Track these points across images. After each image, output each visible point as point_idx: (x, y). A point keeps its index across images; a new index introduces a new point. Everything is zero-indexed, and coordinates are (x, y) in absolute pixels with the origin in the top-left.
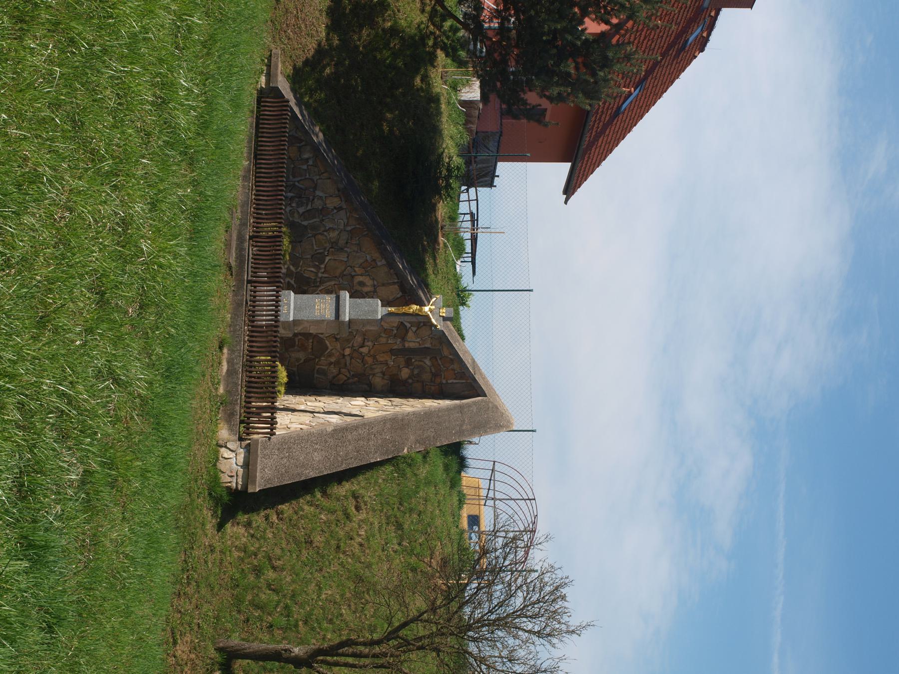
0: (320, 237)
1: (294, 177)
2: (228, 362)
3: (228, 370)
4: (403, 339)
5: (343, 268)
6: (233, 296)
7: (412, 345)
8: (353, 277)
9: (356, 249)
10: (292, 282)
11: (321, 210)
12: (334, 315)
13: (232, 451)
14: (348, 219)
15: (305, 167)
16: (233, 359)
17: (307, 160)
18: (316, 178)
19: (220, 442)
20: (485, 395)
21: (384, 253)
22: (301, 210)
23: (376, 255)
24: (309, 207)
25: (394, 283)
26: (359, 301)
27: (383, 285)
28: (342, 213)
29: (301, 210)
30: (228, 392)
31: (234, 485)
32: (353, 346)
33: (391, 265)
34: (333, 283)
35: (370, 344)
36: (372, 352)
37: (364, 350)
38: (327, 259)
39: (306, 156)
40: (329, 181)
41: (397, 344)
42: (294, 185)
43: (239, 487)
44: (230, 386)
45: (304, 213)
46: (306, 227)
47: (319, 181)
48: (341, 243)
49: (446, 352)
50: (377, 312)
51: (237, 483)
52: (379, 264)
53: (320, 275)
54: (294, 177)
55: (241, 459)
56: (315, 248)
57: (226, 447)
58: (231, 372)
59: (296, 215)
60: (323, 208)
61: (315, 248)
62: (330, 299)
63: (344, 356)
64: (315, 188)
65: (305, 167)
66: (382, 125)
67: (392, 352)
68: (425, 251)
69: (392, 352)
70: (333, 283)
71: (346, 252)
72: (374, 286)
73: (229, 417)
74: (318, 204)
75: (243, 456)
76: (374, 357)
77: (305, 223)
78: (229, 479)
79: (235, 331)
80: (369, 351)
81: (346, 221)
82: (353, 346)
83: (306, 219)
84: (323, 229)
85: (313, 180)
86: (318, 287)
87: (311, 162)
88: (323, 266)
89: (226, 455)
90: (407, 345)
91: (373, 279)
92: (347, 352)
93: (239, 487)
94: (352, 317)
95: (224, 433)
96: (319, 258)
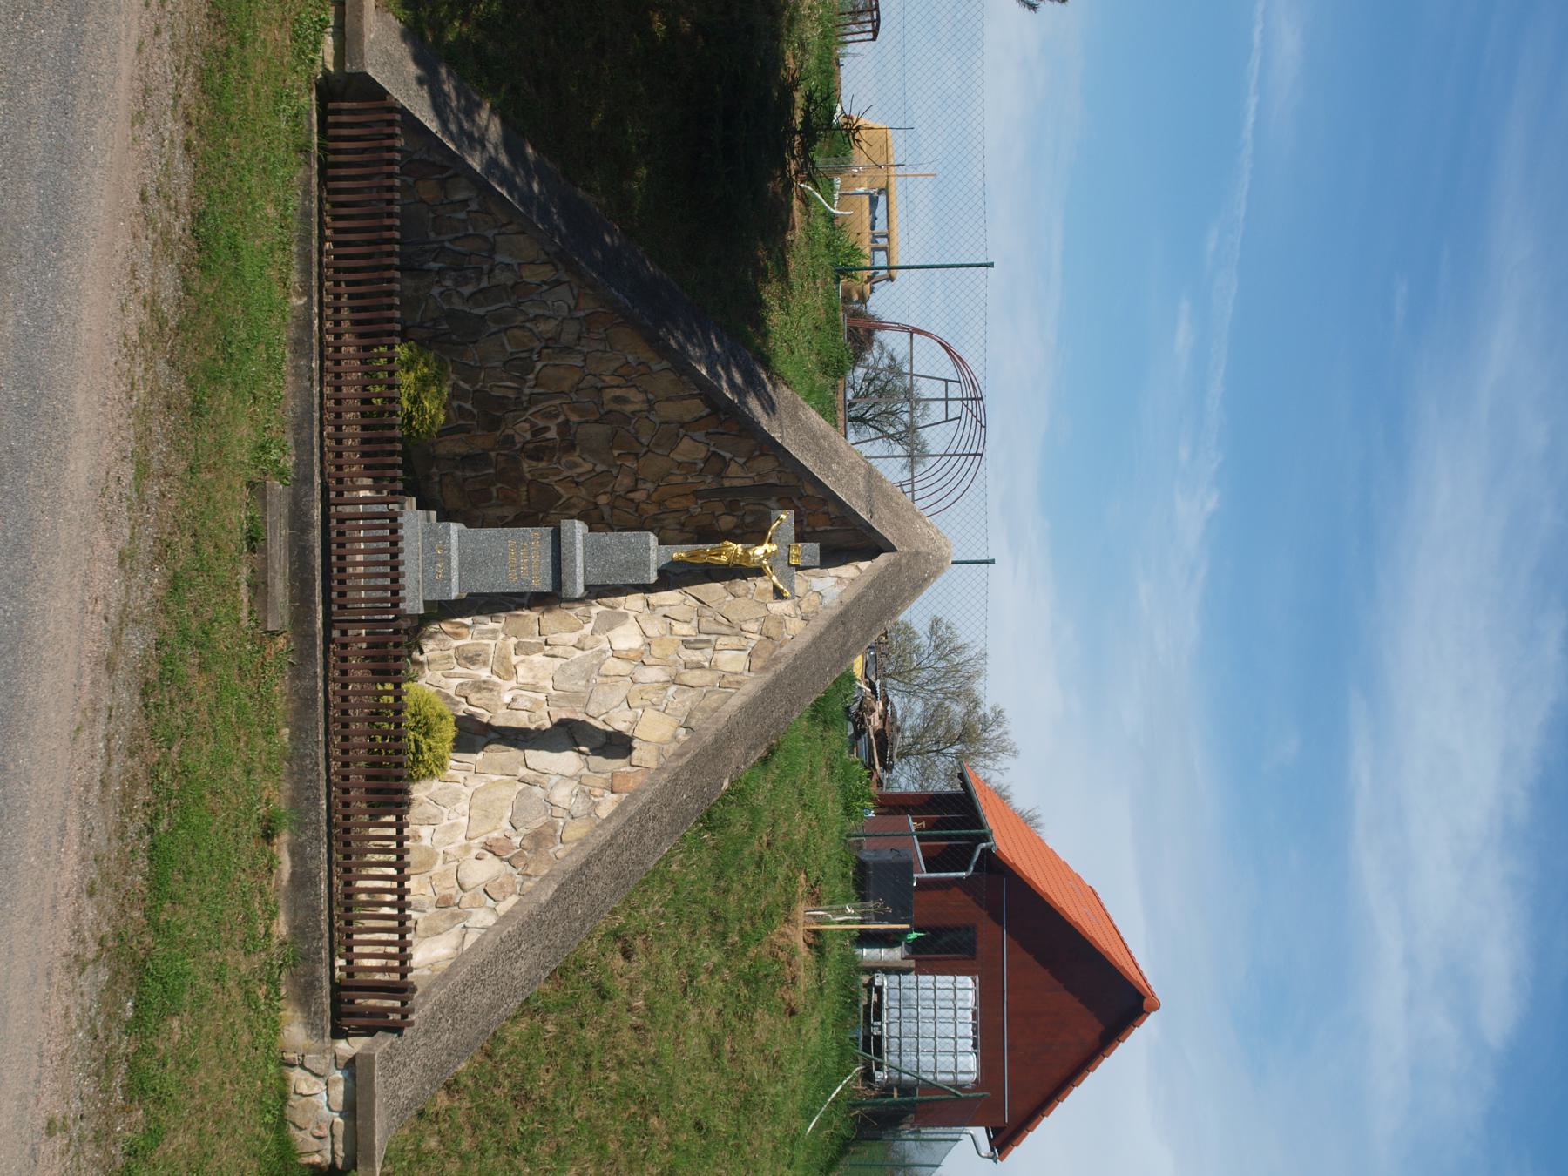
0: (517, 332)
1: (439, 234)
2: (292, 854)
3: (293, 874)
4: (719, 475)
5: (576, 378)
6: (292, 679)
7: (737, 483)
8: (600, 390)
9: (601, 347)
10: (468, 406)
11: (512, 287)
12: (549, 581)
13: (317, 1075)
14: (576, 298)
15: (462, 215)
16: (302, 846)
17: (465, 203)
18: (490, 234)
19: (289, 1056)
20: (892, 549)
21: (663, 350)
22: (467, 290)
23: (647, 355)
24: (484, 284)
25: (692, 396)
26: (607, 538)
27: (668, 399)
28: (563, 291)
29: (467, 290)
30: (298, 930)
31: (329, 1157)
32: (613, 491)
33: (682, 367)
34: (558, 402)
35: (649, 486)
36: (655, 497)
37: (637, 496)
38: (539, 366)
39: (460, 196)
40: (521, 237)
41: (709, 481)
42: (443, 249)
43: (340, 1163)
44: (301, 914)
45: (473, 294)
46: (482, 317)
47: (499, 238)
48: (567, 338)
49: (809, 490)
50: (645, 564)
51: (333, 1152)
52: (656, 367)
53: (527, 391)
54: (439, 234)
55: (338, 1092)
56: (509, 349)
57: (302, 1066)
58: (302, 880)
59: (455, 300)
60: (516, 284)
61: (509, 349)
62: (536, 539)
63: (596, 505)
64: (493, 250)
65: (462, 215)
66: (650, 22)
67: (697, 494)
68: (761, 273)
69: (697, 494)
70: (558, 402)
71: (580, 352)
72: (648, 401)
73: (305, 995)
74: (503, 277)
75: (341, 1088)
76: (660, 503)
77: (481, 311)
78: (314, 1144)
79: (301, 773)
80: (649, 496)
81: (572, 303)
82: (613, 491)
83: (478, 305)
84: (521, 318)
85: (485, 239)
86: (526, 409)
87: (474, 206)
88: (531, 376)
89: (303, 1088)
90: (727, 484)
91: (646, 392)
92: (603, 499)
93: (340, 1163)
94: (592, 581)
95: (295, 1033)
96: (519, 366)
